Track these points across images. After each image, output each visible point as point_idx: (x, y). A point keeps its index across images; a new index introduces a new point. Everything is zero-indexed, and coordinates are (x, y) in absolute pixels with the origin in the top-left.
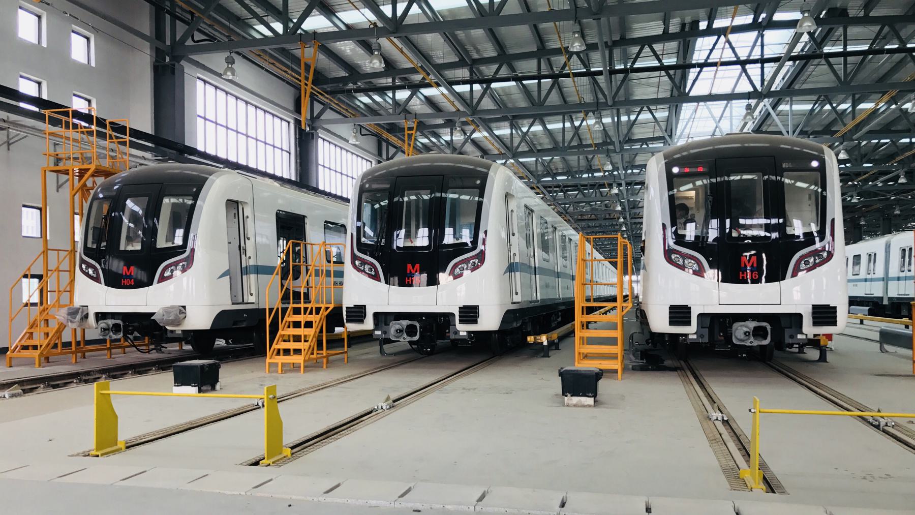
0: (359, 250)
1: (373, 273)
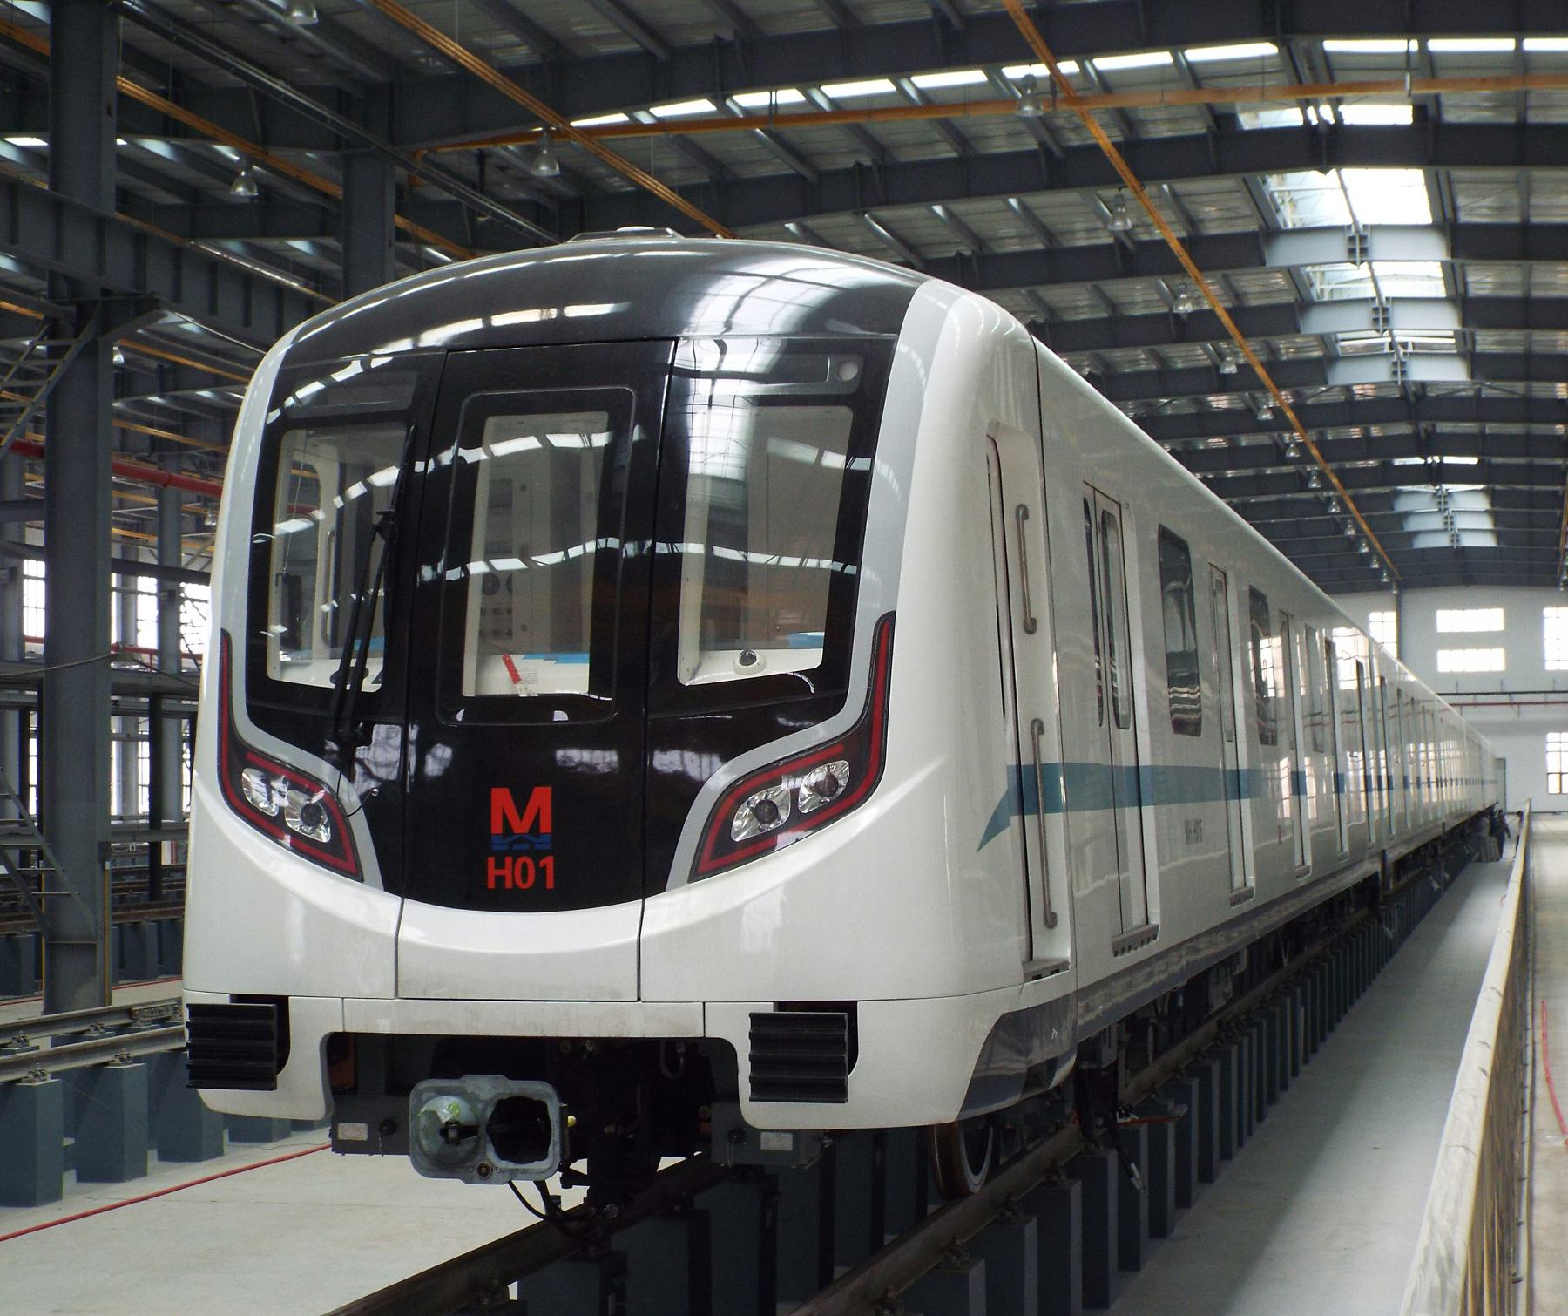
0: (259, 717)
1: (324, 835)
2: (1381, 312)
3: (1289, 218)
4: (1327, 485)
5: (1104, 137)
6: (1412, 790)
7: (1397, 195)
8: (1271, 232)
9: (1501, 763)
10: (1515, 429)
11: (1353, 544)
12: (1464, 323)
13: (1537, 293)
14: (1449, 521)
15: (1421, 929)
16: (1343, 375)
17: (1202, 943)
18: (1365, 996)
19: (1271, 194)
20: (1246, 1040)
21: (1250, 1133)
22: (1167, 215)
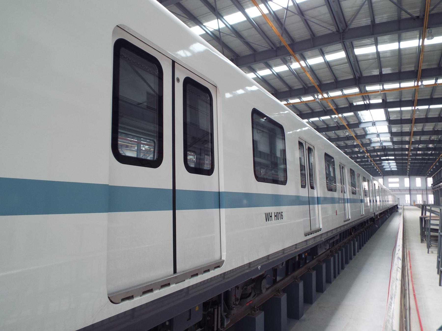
2: (378, 135)
3: (368, 132)
4: (374, 165)
5: (345, 124)
7: (379, 114)
8: (360, 123)
9: (399, 199)
10: (401, 157)
11: (376, 170)
12: (391, 136)
13: (403, 131)
14: (390, 166)
15: (385, 223)
16: (373, 145)
17: (334, 231)
18: (373, 236)
20: (336, 255)
21: (339, 273)
22: (353, 133)
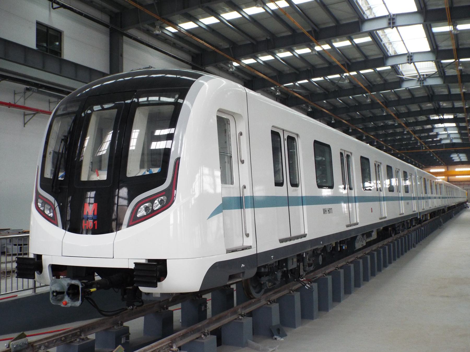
6: (371, 188)
16: (406, 85)
19: (384, 44)
